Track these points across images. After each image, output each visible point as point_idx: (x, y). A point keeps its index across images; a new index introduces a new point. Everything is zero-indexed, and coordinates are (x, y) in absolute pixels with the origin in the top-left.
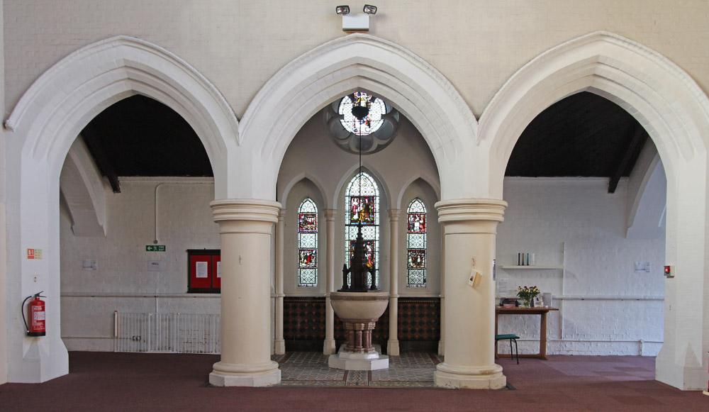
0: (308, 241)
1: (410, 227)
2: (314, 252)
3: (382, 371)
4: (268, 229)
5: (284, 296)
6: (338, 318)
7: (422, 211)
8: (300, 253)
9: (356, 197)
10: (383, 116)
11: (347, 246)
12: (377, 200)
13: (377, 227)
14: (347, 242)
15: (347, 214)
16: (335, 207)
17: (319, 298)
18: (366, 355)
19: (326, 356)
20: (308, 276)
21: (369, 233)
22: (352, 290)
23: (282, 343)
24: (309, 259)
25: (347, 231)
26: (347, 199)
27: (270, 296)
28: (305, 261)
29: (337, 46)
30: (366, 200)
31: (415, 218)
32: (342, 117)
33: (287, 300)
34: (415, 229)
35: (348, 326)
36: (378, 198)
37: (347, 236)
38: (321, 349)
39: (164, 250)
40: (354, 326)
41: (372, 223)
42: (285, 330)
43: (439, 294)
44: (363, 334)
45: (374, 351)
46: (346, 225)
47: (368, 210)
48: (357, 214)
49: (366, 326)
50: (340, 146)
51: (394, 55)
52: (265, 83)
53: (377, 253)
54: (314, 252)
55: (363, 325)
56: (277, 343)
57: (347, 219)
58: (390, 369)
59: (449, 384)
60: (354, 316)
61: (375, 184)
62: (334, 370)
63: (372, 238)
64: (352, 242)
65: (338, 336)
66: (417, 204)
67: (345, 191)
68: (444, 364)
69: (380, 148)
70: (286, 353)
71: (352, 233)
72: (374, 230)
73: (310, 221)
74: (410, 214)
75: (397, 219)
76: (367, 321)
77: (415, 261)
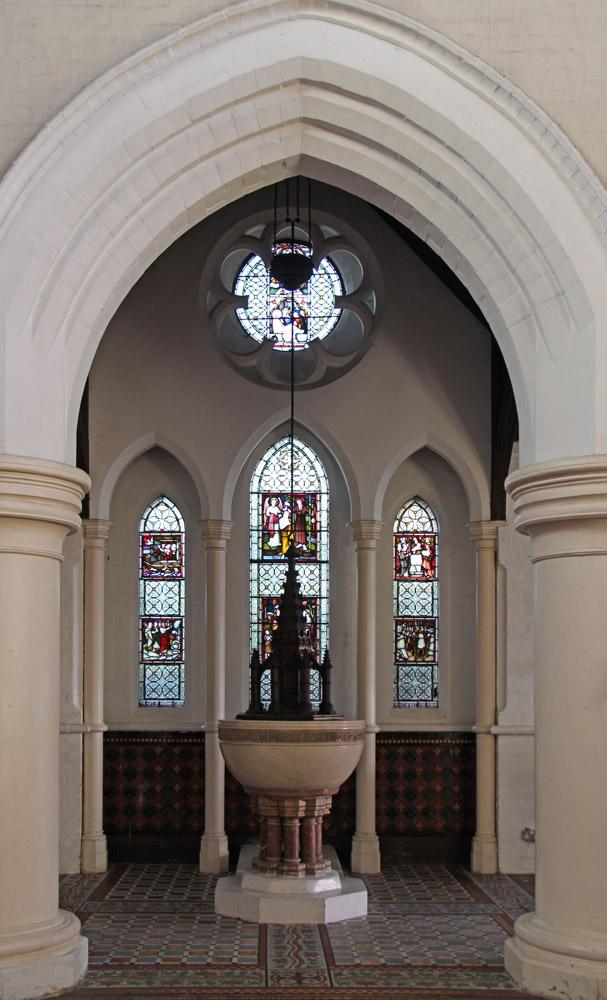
0: (164, 597)
1: (401, 567)
2: (177, 624)
3: (354, 925)
4: (51, 542)
5: (105, 728)
6: (240, 787)
7: (428, 527)
8: (144, 628)
9: (276, 495)
10: (339, 302)
11: (254, 610)
12: (324, 503)
13: (324, 567)
14: (255, 602)
15: (255, 534)
16: (227, 515)
17: (190, 734)
18: (310, 882)
19: (206, 876)
20: (163, 679)
21: (312, 580)
22: (273, 714)
23: (101, 844)
24: (164, 641)
25: (254, 575)
26: (255, 500)
27: (58, 732)
28: (156, 646)
29: (245, 24)
30: (299, 502)
31: (411, 543)
32: (243, 301)
33: (119, 745)
34: (412, 569)
35: (265, 807)
36: (325, 498)
37: (254, 586)
38: (192, 855)
39: (140, 705)
40: (280, 809)
41: (312, 558)
42: (109, 811)
43: (474, 723)
44: (301, 827)
45: (329, 870)
46: (252, 561)
47: (302, 524)
48: (277, 536)
49: (310, 808)
50: (241, 371)
51: (402, 51)
52: (42, 126)
53: (324, 627)
54: (177, 624)
55: (302, 803)
56: (87, 844)
57: (254, 548)
58: (371, 920)
59: (560, 988)
60: (278, 780)
61: (318, 465)
62: (230, 924)
63: (312, 592)
64: (267, 603)
65: (233, 824)
66: (415, 513)
67: (250, 481)
68: (536, 921)
69: (332, 375)
70: (109, 866)
71: (271, 580)
72: (317, 572)
73: (167, 551)
74: (399, 536)
75: (373, 544)
76: (311, 796)
77: (411, 646)
